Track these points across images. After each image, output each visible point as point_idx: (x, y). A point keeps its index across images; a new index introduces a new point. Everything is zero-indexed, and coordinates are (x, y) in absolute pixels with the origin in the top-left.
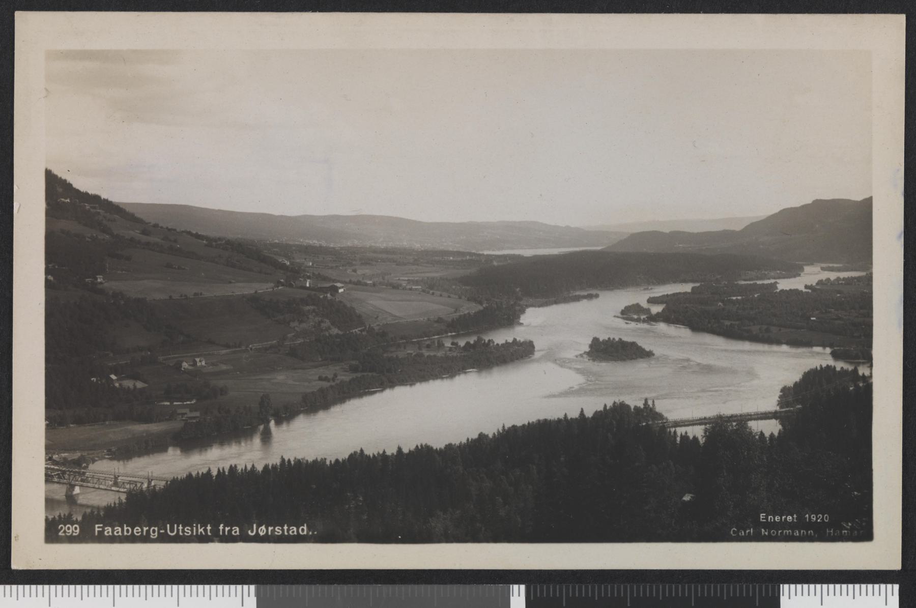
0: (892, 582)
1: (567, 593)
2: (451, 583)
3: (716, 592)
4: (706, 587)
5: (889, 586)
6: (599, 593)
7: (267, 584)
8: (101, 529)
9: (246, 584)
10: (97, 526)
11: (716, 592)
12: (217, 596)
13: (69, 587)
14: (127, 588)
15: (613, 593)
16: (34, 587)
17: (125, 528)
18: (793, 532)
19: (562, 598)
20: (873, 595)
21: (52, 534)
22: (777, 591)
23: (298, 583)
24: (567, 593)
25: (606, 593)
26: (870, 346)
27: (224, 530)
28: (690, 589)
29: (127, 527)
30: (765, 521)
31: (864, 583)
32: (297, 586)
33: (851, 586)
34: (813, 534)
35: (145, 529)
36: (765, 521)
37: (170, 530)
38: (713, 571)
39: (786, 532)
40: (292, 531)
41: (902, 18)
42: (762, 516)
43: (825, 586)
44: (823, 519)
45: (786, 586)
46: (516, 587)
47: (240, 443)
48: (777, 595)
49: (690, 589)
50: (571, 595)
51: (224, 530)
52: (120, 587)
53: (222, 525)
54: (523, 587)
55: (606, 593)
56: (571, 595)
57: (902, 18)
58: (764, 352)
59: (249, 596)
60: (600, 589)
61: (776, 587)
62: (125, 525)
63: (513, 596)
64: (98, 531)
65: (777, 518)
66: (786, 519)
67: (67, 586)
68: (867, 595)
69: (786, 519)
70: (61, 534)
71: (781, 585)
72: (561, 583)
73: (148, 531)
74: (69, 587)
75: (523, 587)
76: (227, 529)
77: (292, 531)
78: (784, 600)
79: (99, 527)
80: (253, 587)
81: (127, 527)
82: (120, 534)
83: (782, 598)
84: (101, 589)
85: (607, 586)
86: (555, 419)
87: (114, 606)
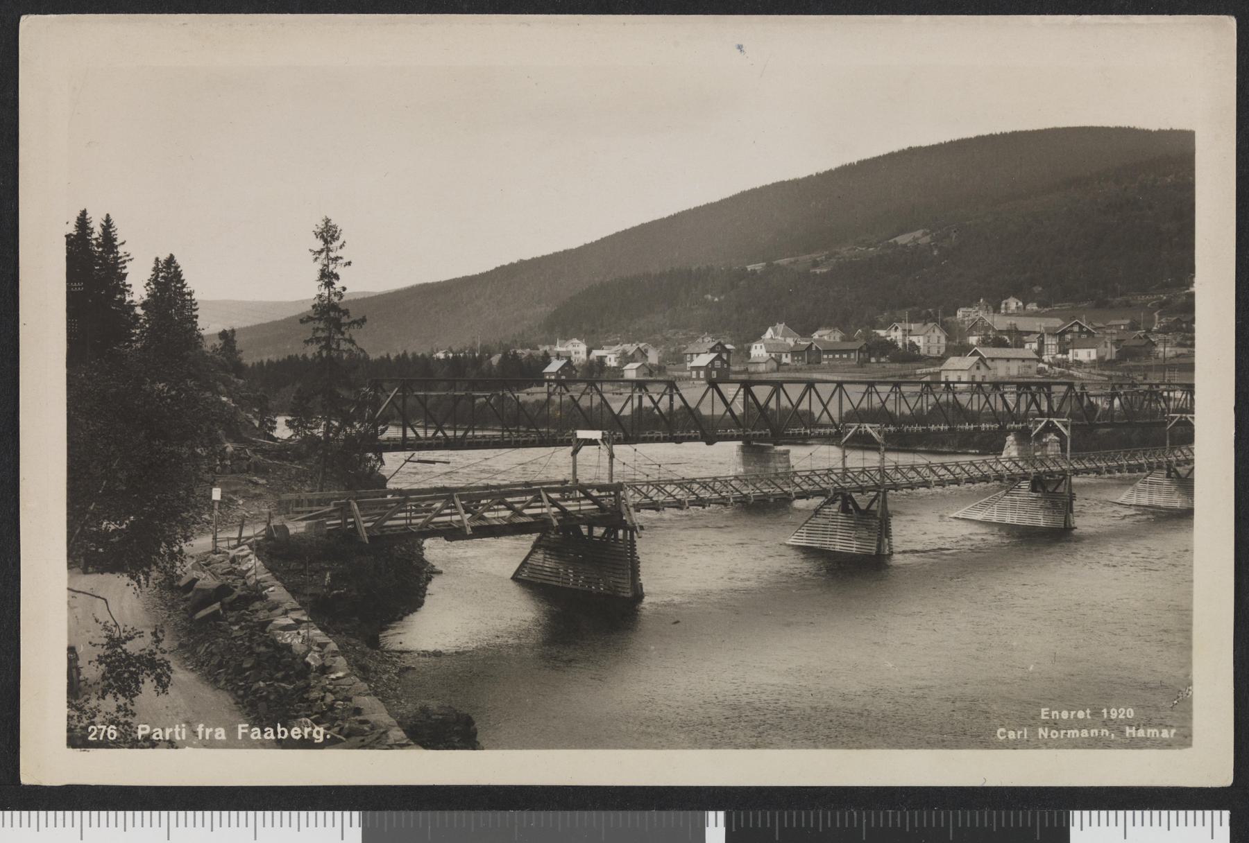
0: (1220, 807)
2: (491, 808)
3: (764, 822)
5: (1217, 813)
6: (912, 821)
7: (463, 810)
8: (246, 731)
9: (1156, 809)
11: (764, 822)
12: (177, 826)
13: (90, 814)
14: (99, 814)
15: (1016, 822)
16: (190, 813)
17: (279, 729)
18: (1160, 733)
21: (77, 740)
22: (1064, 816)
25: (964, 822)
26: (68, 376)
27: (204, 733)
28: (1034, 817)
30: (1047, 718)
33: (1121, 813)
34: (1107, 734)
35: (307, 730)
36: (1047, 718)
39: (1151, 733)
40: (156, 734)
41: (1230, 23)
42: (1044, 711)
43: (1173, 813)
44: (1125, 715)
45: (1077, 813)
46: (711, 814)
48: (1064, 825)
49: (1034, 817)
51: (204, 733)
52: (238, 814)
53: (201, 726)
54: (721, 814)
55: (964, 822)
57: (1230, 23)
58: (1112, 484)
60: (956, 816)
63: (1073, 825)
64: (243, 733)
65: (1065, 715)
66: (1076, 714)
67: (105, 812)
68: (1108, 825)
69: (1076, 714)
70: (90, 738)
71: (1071, 812)
72: (912, 809)
74: (221, 814)
75: (721, 814)
76: (208, 731)
77: (156, 734)
78: (1074, 831)
79: (243, 728)
80: (356, 814)
82: (161, 738)
87: (82, 839)
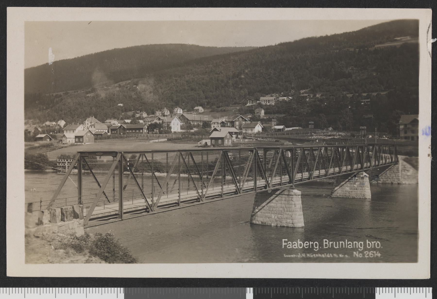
0: (429, 286)
1: (335, 292)
3: (282, 291)
4: (352, 289)
5: (427, 288)
10: (283, 240)
11: (282, 291)
13: (80, 289)
19: (332, 294)
20: (423, 293)
23: (135, 287)
24: (335, 292)
25: (338, 292)
28: (363, 290)
29: (368, 241)
31: (406, 287)
32: (146, 288)
37: (343, 244)
38: (332, 279)
43: (412, 288)
45: (378, 288)
46: (248, 289)
47: (78, 57)
48: (373, 293)
50: (352, 293)
54: (252, 289)
56: (352, 293)
59: (120, 293)
61: (373, 288)
62: (367, 240)
73: (312, 245)
74: (3, 289)
75: (252, 289)
78: (377, 295)
80: (122, 289)
81: (368, 241)
83: (376, 294)
84: (108, 289)
85: (255, 288)
86: (316, 37)
